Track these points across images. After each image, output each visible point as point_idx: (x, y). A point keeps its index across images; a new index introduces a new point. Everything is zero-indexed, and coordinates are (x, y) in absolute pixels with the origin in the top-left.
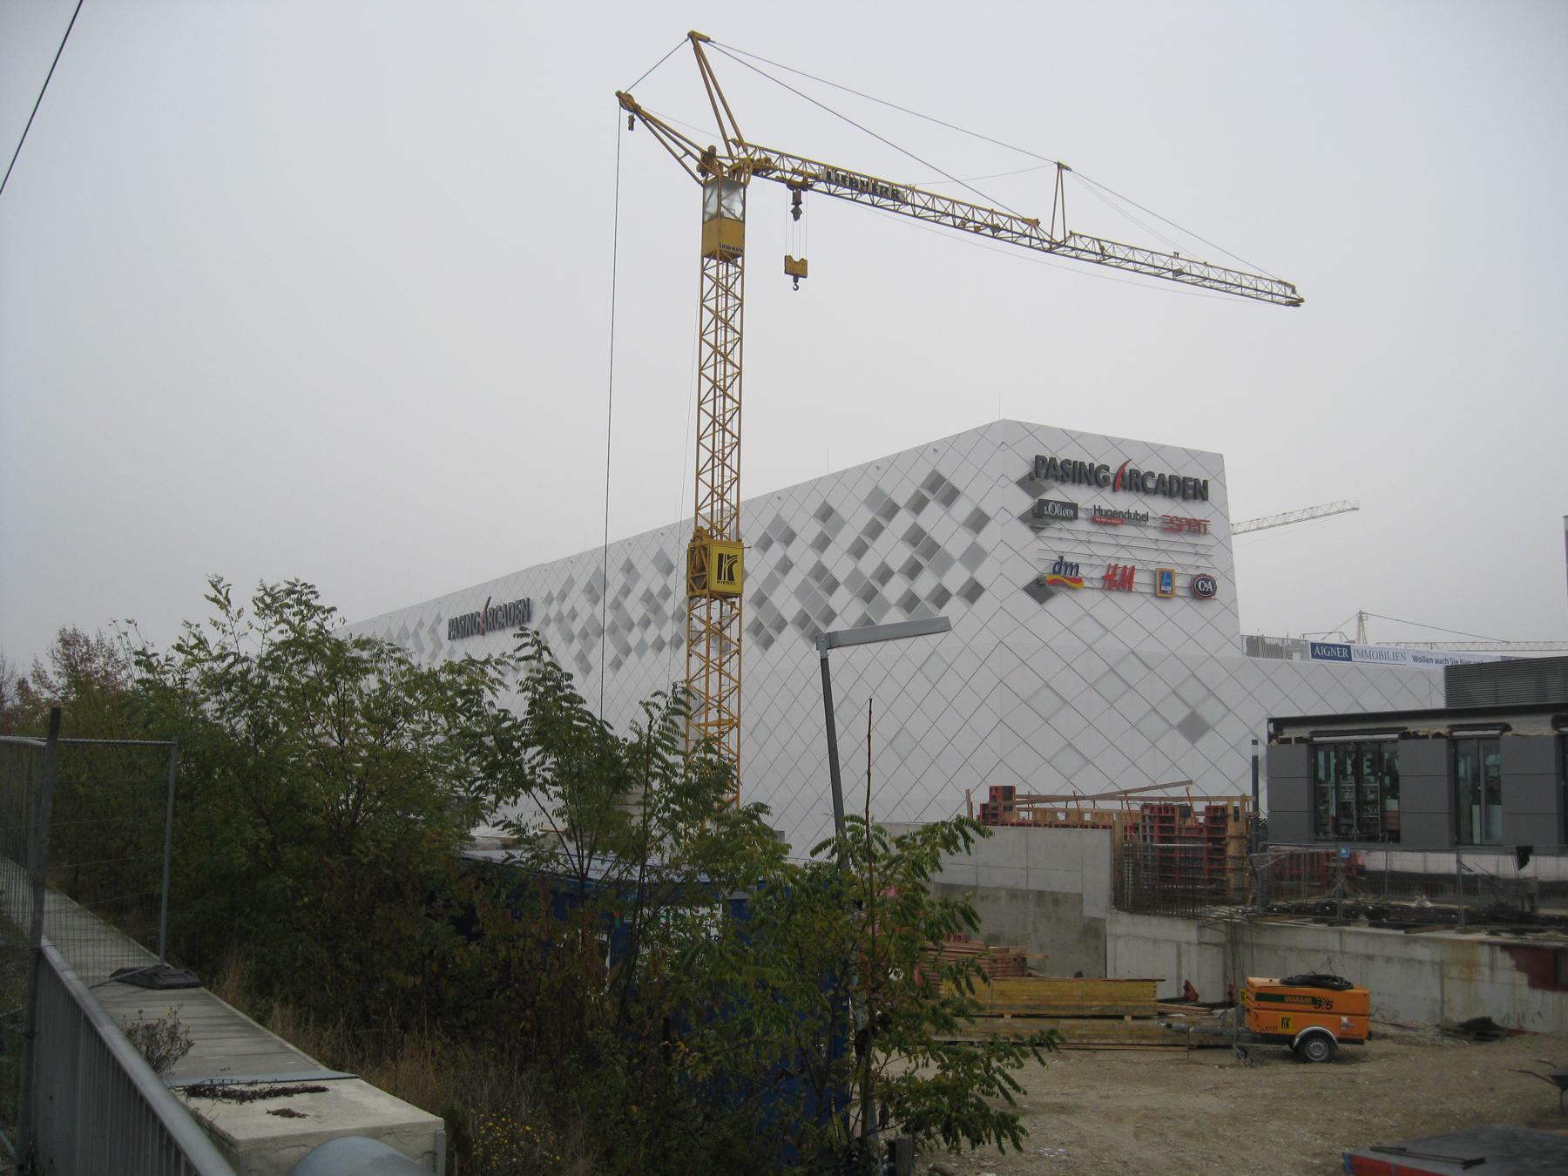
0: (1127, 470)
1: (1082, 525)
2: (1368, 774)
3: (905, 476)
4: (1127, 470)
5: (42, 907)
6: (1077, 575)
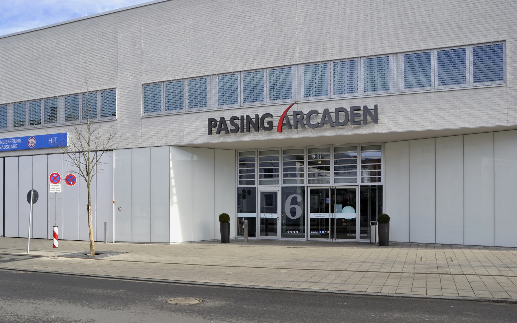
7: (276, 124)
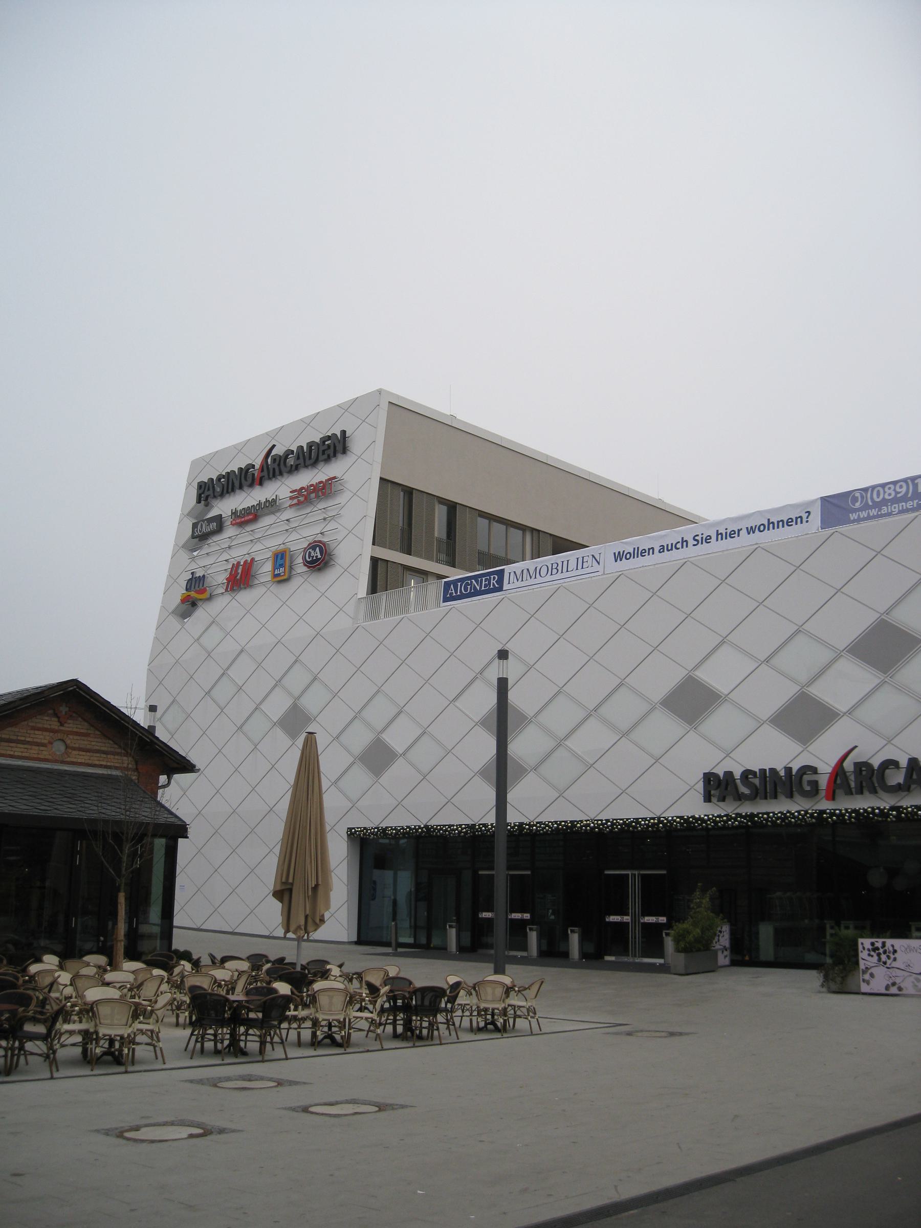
0: (848, 765)
1: (230, 532)
2: (869, 513)
3: (208, 463)
4: (848, 765)
5: (83, 763)
6: (203, 586)
7: (823, 782)
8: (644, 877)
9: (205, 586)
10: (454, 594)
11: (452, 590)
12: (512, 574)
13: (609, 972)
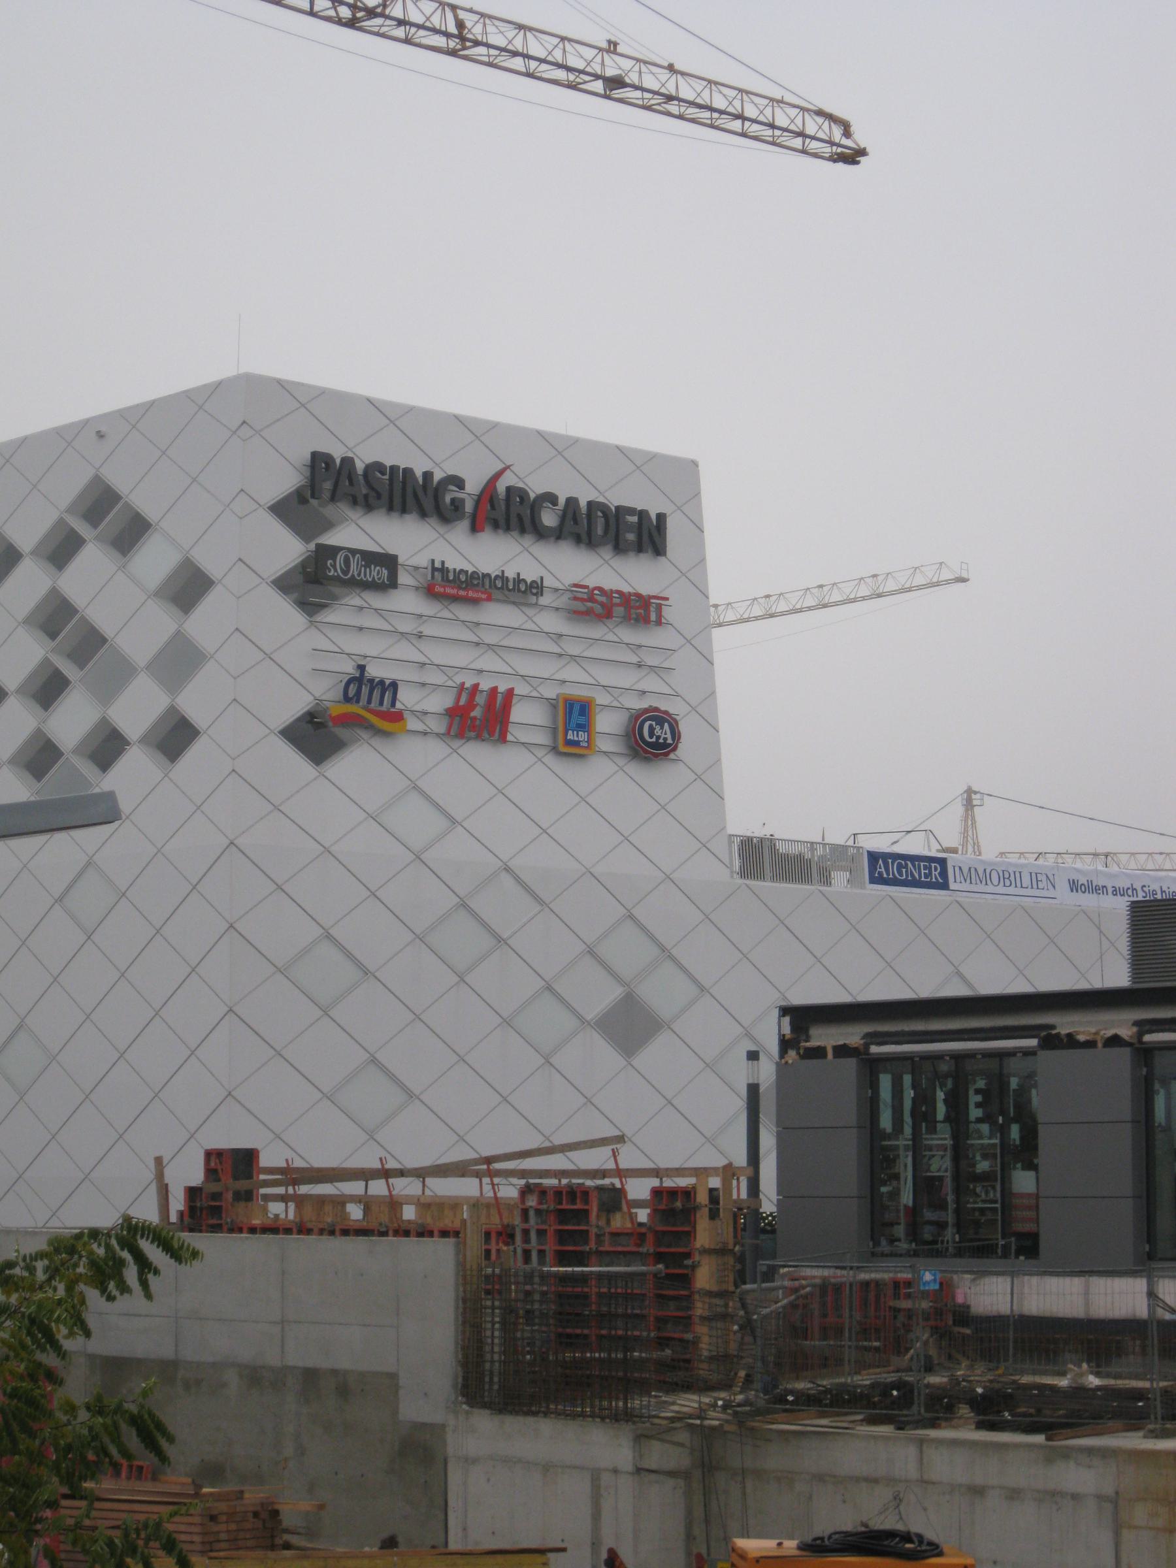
0: (501, 487)
4: (501, 487)
6: (393, 704)
8: (997, 1171)
9: (398, 705)
10: (885, 876)
11: (880, 868)
12: (957, 869)
13: (1061, 1315)
